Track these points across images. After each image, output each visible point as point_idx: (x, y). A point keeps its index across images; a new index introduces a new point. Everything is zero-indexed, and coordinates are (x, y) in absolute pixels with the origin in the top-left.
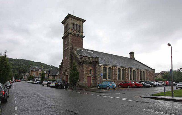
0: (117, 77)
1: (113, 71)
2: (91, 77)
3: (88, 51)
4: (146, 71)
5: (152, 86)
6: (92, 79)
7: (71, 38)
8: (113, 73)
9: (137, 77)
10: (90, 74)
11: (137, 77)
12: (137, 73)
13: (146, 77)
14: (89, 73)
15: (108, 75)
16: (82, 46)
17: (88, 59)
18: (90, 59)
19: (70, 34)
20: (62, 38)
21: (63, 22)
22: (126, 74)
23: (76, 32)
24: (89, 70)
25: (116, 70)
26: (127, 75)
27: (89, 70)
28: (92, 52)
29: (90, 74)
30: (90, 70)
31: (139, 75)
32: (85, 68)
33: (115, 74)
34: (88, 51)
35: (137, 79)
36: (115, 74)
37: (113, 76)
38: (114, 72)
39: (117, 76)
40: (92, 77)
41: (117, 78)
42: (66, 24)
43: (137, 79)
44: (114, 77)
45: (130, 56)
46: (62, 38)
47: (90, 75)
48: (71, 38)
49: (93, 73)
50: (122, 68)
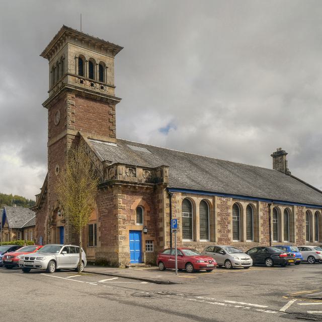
0: (229, 231)
1: (217, 210)
11: (296, 231)
12: (296, 217)
23: (92, 85)
26: (263, 225)
31: (305, 224)
35: (296, 238)
42: (56, 58)
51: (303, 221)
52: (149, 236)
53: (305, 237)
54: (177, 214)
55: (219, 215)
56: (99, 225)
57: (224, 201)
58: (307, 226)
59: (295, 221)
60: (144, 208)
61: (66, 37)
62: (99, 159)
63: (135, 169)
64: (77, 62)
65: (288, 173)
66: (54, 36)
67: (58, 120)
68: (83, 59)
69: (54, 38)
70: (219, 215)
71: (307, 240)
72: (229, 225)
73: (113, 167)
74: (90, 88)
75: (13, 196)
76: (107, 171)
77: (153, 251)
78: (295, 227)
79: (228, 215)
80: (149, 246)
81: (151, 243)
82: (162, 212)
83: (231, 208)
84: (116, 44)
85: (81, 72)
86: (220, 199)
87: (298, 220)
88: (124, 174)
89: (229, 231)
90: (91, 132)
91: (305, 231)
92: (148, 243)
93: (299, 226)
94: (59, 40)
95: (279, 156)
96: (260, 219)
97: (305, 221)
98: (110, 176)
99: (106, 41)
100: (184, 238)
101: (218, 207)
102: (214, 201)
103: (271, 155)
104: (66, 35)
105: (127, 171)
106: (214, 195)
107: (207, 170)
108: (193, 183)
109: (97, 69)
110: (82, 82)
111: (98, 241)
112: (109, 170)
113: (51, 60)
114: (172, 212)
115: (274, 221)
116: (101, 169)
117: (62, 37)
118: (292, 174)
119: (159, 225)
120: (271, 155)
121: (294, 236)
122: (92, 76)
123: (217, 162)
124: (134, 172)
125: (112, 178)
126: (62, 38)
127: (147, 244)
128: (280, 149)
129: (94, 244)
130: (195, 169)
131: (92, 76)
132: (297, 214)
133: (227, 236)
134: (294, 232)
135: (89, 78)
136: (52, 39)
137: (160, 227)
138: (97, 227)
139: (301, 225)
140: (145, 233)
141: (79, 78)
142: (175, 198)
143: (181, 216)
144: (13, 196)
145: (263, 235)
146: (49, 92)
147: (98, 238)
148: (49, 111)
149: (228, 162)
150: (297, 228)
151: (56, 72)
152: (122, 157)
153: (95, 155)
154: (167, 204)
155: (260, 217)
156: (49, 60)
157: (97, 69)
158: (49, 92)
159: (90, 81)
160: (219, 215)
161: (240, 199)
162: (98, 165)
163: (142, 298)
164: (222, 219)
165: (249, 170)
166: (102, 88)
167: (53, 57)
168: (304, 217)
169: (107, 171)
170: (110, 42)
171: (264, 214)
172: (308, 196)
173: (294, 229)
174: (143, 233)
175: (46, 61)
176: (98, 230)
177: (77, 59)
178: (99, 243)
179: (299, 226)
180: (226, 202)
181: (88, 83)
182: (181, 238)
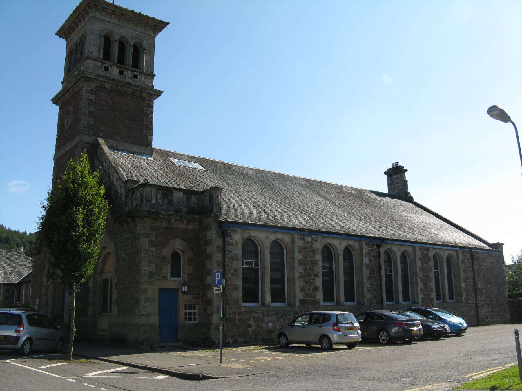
0: (316, 289)
1: (298, 256)
2: (176, 290)
3: (176, 162)
4: (461, 257)
5: (438, 318)
6: (183, 300)
7: (93, 97)
8: (299, 269)
9: (420, 285)
10: (176, 273)
11: (420, 285)
12: (419, 264)
13: (463, 285)
14: (167, 269)
15: (268, 281)
16: (150, 144)
17: (164, 196)
18: (175, 200)
19: (88, 80)
20: (55, 101)
21: (63, 33)
22: (366, 272)
23: (121, 73)
24: (169, 255)
25: (314, 252)
26: (369, 278)
27: (167, 252)
28: (197, 166)
29: (176, 273)
30: (175, 257)
31: (432, 275)
32: (145, 243)
33: (426, 280)
34: (176, 162)
35: (421, 296)
36: (426, 280)
37: (299, 283)
38: (301, 263)
39: (319, 282)
40: (185, 289)
41: (320, 295)
42: (75, 37)
43: (421, 296)
44: (302, 290)
45: (390, 185)
46: (55, 101)
47: (172, 283)
48: (93, 97)
49: (185, 268)
50: (345, 244)
51: (430, 269)
52: (190, 297)
53: (433, 295)
54: (234, 262)
55: (301, 263)
56: (115, 281)
57: (308, 242)
58: (437, 278)
59: (418, 270)
60: (183, 253)
61: (90, 11)
62: (120, 179)
63: (172, 192)
64: (102, 43)
65: (409, 199)
66: (74, 8)
67: (70, 122)
68: (111, 38)
69: (74, 11)
70: (301, 263)
71: (438, 298)
72: (317, 279)
73: (138, 190)
74: (118, 77)
75: (28, 234)
76: (130, 196)
77: (197, 322)
78: (419, 280)
79: (315, 262)
80: (190, 314)
81: (194, 308)
82: (210, 259)
83: (320, 252)
84: (159, 18)
85: (107, 56)
86: (303, 239)
87: (422, 269)
88: (154, 201)
89: (316, 289)
90: (115, 139)
91: (433, 285)
92: (190, 309)
93: (424, 278)
94: (81, 14)
95: (396, 173)
96: (364, 268)
97: (433, 270)
98: (134, 204)
99: (138, 12)
100: (244, 301)
101: (299, 251)
102: (293, 242)
103: (385, 173)
104: (89, 8)
105: (159, 196)
106: (293, 232)
107: (288, 194)
108: (262, 215)
109: (130, 51)
110: (106, 69)
111: (113, 305)
112: (133, 194)
113: (69, 39)
114: (227, 260)
115: (386, 270)
116: (123, 193)
117: (84, 9)
118: (415, 200)
119: (206, 279)
120: (385, 173)
121: (417, 293)
122: (121, 61)
123: (304, 183)
124: (170, 198)
125: (136, 206)
126: (84, 11)
127: (188, 311)
128: (397, 163)
129: (108, 311)
130: (267, 193)
131: (121, 61)
132: (420, 259)
133: (315, 297)
134: (417, 287)
135: (118, 63)
136: (72, 12)
137: (208, 283)
138: (114, 283)
139: (427, 276)
140: (184, 293)
141: (103, 63)
142: (230, 236)
143: (240, 266)
144: (28, 234)
145: (422, 283)
146: (62, 83)
147: (113, 299)
148: (60, 109)
149: (321, 183)
150: (422, 280)
151: (73, 55)
152: (156, 176)
153: (116, 172)
154: (218, 248)
155: (364, 265)
156: (66, 40)
157: (130, 51)
158: (62, 83)
159: (119, 67)
160: (301, 263)
161: (333, 238)
162: (119, 187)
163: (266, 374)
164: (305, 270)
165: (353, 195)
166: (135, 77)
167: (72, 36)
168: (431, 264)
169: (130, 196)
170: (150, 16)
171: (370, 261)
172: (436, 232)
173: (417, 283)
174: (180, 294)
175: (63, 42)
176: (114, 287)
177: (103, 39)
178: (114, 309)
179: (424, 278)
180: (312, 243)
181: (129, 73)
182: (241, 300)
